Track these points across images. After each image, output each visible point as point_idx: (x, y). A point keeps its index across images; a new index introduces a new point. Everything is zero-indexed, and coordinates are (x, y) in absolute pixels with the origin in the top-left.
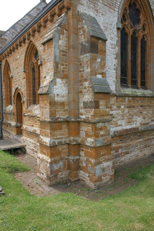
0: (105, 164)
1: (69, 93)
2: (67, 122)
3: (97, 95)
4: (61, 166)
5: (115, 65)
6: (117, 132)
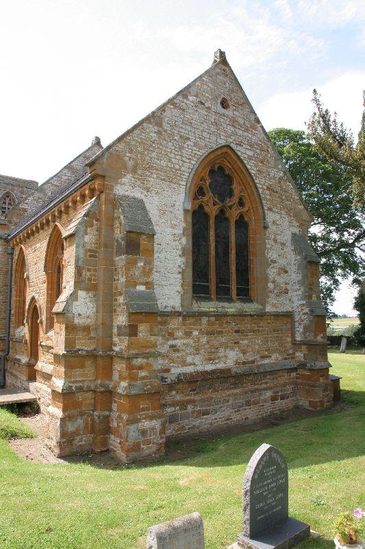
0: (146, 424)
1: (97, 312)
2: (92, 355)
3: (133, 317)
4: (79, 426)
5: (180, 266)
6: (185, 374)
